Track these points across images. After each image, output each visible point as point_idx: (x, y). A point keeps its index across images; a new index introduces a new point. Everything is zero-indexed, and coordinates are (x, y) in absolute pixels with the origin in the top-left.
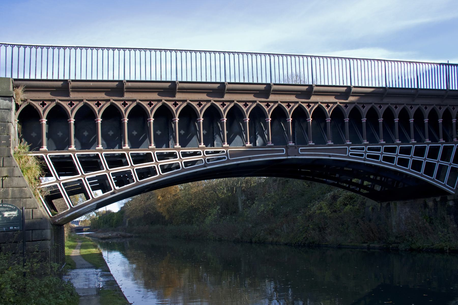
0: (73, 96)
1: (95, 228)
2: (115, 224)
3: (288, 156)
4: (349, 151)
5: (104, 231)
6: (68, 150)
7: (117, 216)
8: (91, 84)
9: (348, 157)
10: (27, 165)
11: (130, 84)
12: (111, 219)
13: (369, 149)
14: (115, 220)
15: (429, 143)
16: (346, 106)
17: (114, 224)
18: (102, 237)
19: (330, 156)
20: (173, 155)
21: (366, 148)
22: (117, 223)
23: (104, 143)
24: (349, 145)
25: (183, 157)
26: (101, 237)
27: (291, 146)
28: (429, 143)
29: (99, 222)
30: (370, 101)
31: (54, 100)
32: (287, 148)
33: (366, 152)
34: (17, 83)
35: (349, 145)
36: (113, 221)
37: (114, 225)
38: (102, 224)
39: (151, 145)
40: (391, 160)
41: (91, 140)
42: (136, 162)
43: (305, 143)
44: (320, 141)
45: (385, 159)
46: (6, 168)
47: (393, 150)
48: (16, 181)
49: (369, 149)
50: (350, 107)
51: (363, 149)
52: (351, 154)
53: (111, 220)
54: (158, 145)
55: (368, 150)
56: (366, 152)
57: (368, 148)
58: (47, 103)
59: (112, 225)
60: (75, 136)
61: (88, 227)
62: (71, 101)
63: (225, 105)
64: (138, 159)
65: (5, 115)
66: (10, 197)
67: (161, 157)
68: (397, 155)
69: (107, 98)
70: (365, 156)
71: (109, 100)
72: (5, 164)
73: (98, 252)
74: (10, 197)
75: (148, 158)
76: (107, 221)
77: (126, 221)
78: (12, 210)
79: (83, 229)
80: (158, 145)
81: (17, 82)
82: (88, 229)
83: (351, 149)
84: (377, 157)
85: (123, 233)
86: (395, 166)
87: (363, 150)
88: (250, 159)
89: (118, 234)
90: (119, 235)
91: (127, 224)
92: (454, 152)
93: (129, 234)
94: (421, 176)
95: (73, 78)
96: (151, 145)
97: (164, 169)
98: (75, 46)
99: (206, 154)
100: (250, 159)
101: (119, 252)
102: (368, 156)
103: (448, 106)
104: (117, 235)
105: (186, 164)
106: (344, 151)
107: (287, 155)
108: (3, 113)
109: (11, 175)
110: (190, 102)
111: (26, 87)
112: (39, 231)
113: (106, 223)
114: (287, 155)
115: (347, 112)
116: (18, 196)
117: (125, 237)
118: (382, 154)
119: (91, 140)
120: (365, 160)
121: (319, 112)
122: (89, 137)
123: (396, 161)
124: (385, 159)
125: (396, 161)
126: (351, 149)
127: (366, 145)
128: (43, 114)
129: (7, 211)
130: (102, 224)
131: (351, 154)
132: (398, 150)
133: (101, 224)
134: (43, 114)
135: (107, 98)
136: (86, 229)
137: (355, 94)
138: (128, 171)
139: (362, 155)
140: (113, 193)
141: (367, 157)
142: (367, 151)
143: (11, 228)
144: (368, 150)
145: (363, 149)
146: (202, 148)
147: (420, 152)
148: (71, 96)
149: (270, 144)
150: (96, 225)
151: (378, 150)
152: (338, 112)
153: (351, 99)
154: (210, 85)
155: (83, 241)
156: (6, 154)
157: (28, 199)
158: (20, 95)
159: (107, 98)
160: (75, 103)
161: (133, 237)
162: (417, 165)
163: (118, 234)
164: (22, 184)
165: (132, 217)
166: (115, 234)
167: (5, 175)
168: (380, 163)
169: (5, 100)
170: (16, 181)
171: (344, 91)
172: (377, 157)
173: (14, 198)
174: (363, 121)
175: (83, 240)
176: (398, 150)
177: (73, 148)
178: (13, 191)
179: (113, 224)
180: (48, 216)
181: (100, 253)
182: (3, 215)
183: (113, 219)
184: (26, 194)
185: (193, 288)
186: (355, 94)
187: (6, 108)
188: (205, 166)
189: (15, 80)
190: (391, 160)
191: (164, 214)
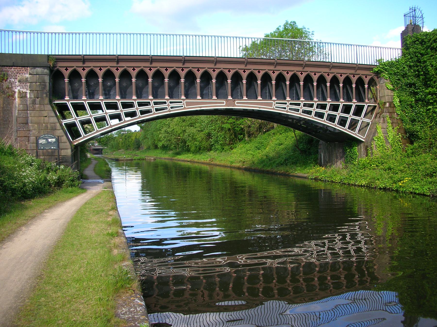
4: (275, 105)
6: (64, 99)
9: (273, 109)
13: (291, 104)
15: (356, 103)
24: (274, 101)
28: (356, 103)
33: (288, 106)
35: (274, 101)
40: (309, 113)
42: (323, 114)
44: (252, 95)
45: (304, 112)
47: (312, 106)
49: (291, 104)
51: (286, 104)
52: (276, 107)
55: (155, 104)
56: (288, 106)
57: (290, 103)
64: (125, 106)
67: (140, 104)
70: (287, 109)
78: (53, 138)
83: (276, 103)
84: (298, 110)
86: (312, 117)
98: (86, 32)
100: (260, 108)
102: (290, 109)
106: (271, 104)
118: (301, 108)
120: (287, 112)
123: (313, 114)
124: (304, 112)
125: (313, 114)
126: (276, 103)
127: (288, 101)
129: (50, 138)
132: (315, 106)
138: (60, 104)
139: (285, 108)
142: (303, 107)
144: (155, 104)
147: (335, 108)
151: (299, 105)
162: (332, 118)
168: (300, 114)
169: (45, 69)
172: (298, 110)
176: (315, 106)
177: (67, 98)
182: (48, 141)
190: (309, 113)
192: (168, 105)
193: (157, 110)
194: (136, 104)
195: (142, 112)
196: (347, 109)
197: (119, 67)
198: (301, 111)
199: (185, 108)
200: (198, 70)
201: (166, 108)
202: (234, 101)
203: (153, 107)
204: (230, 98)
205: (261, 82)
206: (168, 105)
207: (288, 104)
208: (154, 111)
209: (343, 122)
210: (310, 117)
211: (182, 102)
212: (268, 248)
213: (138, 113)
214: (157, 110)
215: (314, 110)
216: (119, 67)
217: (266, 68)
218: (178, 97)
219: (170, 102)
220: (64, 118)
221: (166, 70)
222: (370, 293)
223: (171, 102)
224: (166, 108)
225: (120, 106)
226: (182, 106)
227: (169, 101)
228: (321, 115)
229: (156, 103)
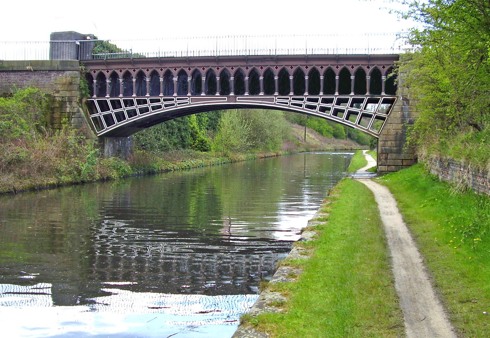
9: (275, 104)
20: (159, 101)
24: (276, 96)
27: (232, 96)
30: (267, 64)
35: (276, 96)
40: (147, 110)
45: (308, 107)
47: (316, 100)
54: (165, 95)
64: (139, 102)
67: (152, 101)
68: (319, 104)
75: (145, 102)
80: (98, 96)
83: (278, 98)
84: (301, 105)
87: (288, 99)
92: (261, 103)
97: (154, 108)
99: (177, 100)
103: (239, 66)
124: (308, 107)
139: (287, 103)
151: (302, 100)
154: (119, 60)
168: (303, 109)
174: (203, 79)
185: (25, 169)
192: (290, 101)
193: (166, 106)
194: (162, 100)
195: (154, 108)
196: (104, 106)
197: (339, 65)
198: (304, 106)
199: (190, 104)
200: (232, 68)
201: (174, 105)
202: (236, 97)
203: (162, 103)
204: (232, 94)
205: (263, 78)
206: (176, 102)
207: (305, 99)
208: (163, 106)
209: (109, 120)
210: (149, 113)
211: (187, 99)
212: (455, 247)
213: (150, 109)
214: (166, 106)
215: (319, 104)
216: (339, 65)
217: (127, 67)
218: (287, 93)
219: (177, 99)
220: (92, 113)
221: (322, 67)
222: (10, 289)
223: (178, 99)
224: (174, 105)
225: (135, 103)
226: (188, 103)
227: (176, 98)
229: (165, 100)
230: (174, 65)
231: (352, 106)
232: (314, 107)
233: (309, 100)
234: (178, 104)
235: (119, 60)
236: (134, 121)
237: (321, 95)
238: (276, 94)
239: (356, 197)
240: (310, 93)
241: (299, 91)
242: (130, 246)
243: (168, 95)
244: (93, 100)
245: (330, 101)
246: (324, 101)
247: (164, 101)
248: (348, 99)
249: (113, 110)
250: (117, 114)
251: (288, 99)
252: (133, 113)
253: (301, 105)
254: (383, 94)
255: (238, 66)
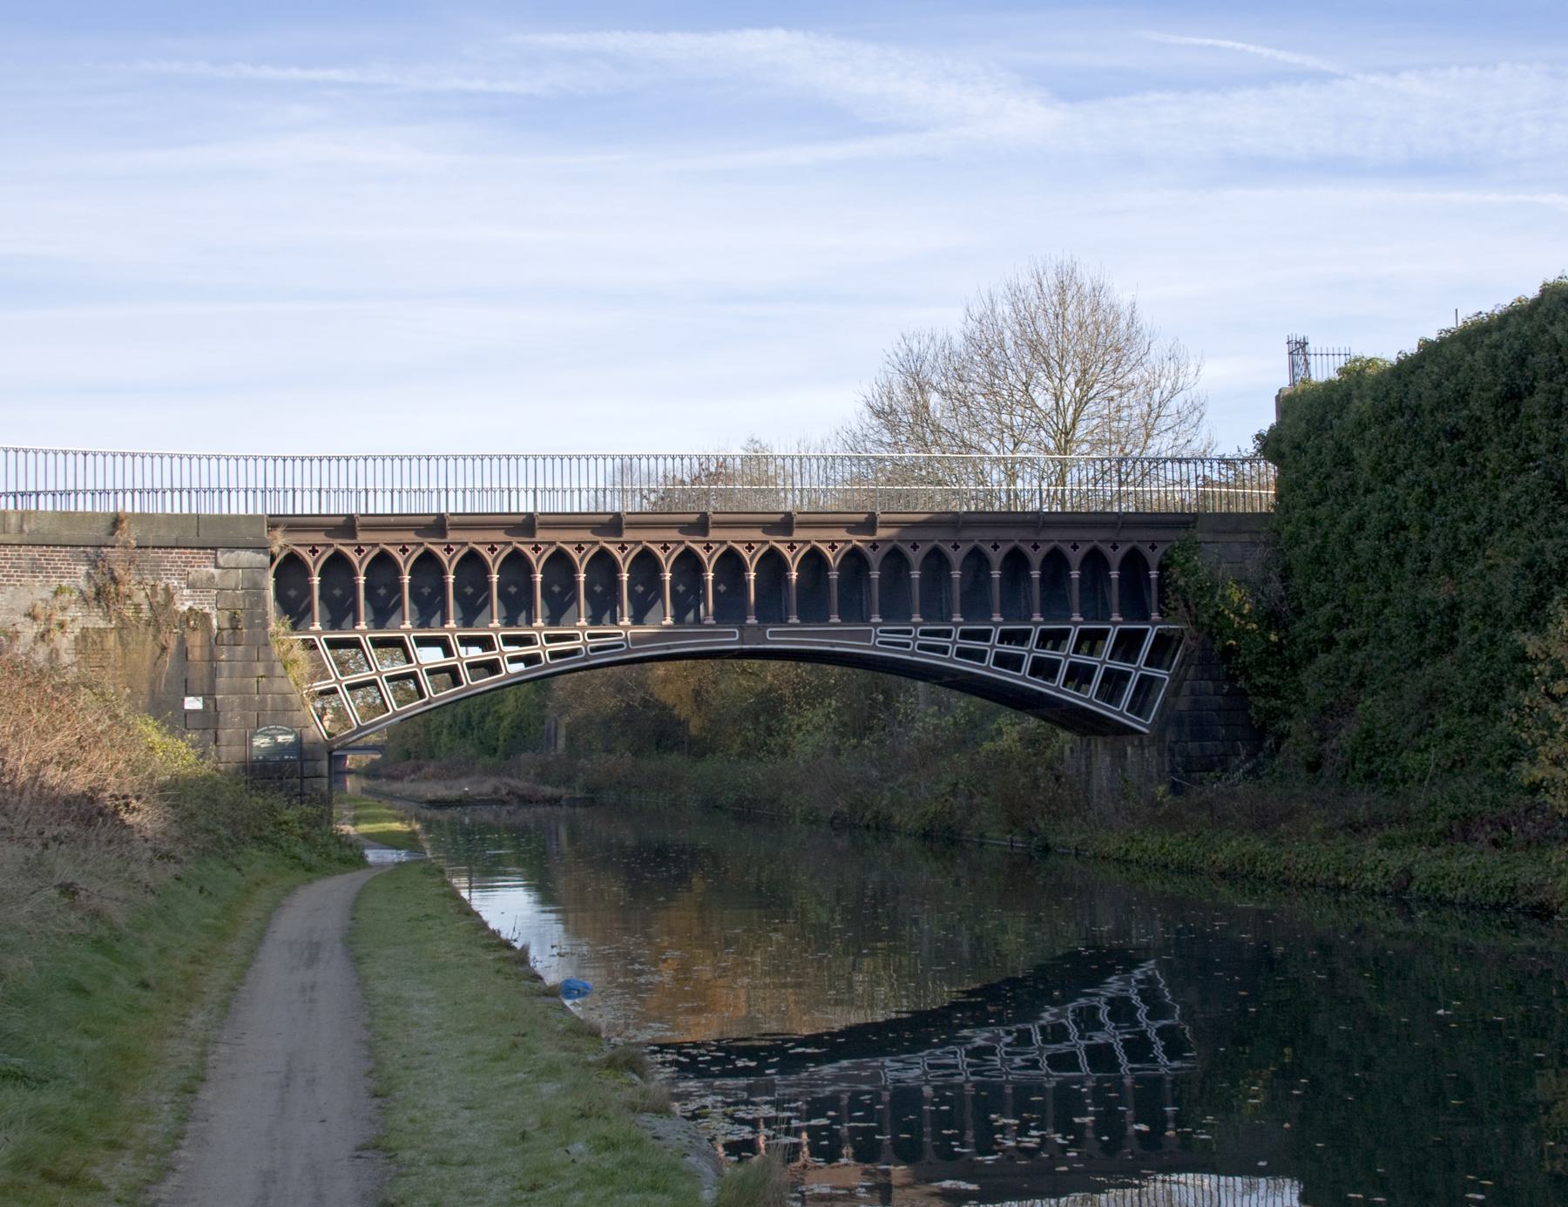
0: (362, 537)
1: (408, 756)
2: (505, 741)
3: (744, 644)
4: (877, 636)
5: (451, 772)
7: (517, 701)
8: (392, 519)
9: (874, 647)
10: (290, 656)
11: (456, 518)
12: (488, 713)
13: (923, 633)
14: (509, 719)
16: (874, 547)
17: (501, 738)
18: (433, 798)
19: (832, 645)
21: (916, 631)
22: (514, 737)
23: (415, 607)
24: (876, 625)
25: (547, 642)
26: (430, 796)
27: (751, 626)
29: (433, 727)
31: (332, 545)
32: (741, 629)
33: (915, 639)
34: (274, 522)
35: (876, 625)
36: (498, 725)
37: (501, 742)
38: (444, 738)
39: (492, 622)
41: (393, 602)
43: (783, 621)
45: (962, 653)
46: (262, 664)
47: (984, 636)
48: (278, 684)
49: (923, 633)
50: (884, 549)
52: (880, 643)
53: (489, 719)
56: (915, 639)
58: (320, 550)
59: (494, 743)
60: (366, 598)
61: (374, 748)
62: (359, 545)
63: (626, 548)
65: (259, 578)
66: (269, 708)
68: (993, 647)
69: (419, 540)
70: (914, 646)
71: (422, 544)
72: (261, 656)
73: (408, 829)
74: (269, 708)
76: (469, 723)
77: (556, 728)
78: (287, 733)
79: (344, 757)
81: (273, 519)
82: (373, 761)
83: (881, 632)
84: (945, 650)
85: (521, 785)
88: (668, 647)
89: (503, 787)
90: (504, 792)
91: (561, 743)
93: (548, 790)
94: (1057, 692)
95: (363, 512)
96: (492, 622)
100: (668, 647)
101: (553, 916)
102: (921, 647)
104: (496, 790)
105: (554, 655)
106: (866, 636)
107: (742, 641)
108: (256, 574)
109: (270, 674)
110: (562, 545)
111: (289, 526)
112: (312, 763)
113: (464, 734)
114: (742, 641)
115: (875, 558)
116: (281, 708)
117: (531, 802)
119: (393, 602)
121: (814, 560)
122: (388, 597)
124: (962, 653)
126: (881, 632)
127: (916, 625)
128: (314, 568)
129: (281, 734)
130: (444, 738)
131: (880, 643)
132: (995, 636)
133: (439, 734)
134: (314, 568)
135: (419, 539)
136: (358, 757)
137: (887, 525)
139: (907, 645)
140: (428, 703)
141: (919, 648)
143: (286, 757)
145: (909, 632)
146: (582, 628)
147: (1053, 638)
148: (359, 538)
149: (711, 621)
150: (416, 740)
151: (948, 634)
152: (855, 556)
153: (882, 533)
155: (356, 807)
156: (262, 641)
157: (295, 713)
158: (280, 542)
159: (419, 540)
160: (366, 549)
161: (562, 802)
163: (503, 787)
164: (286, 688)
165: (580, 711)
166: (487, 786)
167: (262, 674)
168: (951, 660)
170: (278, 684)
171: (863, 520)
173: (275, 710)
175: (358, 804)
176: (995, 636)
178: (273, 699)
179: (498, 739)
180: (320, 736)
181: (410, 833)
182: (276, 740)
183: (496, 712)
184: (292, 705)
186: (887, 525)
187: (259, 566)
188: (585, 660)
189: (271, 516)
191: (683, 711)
204: (752, 620)
228: (1012, 662)
229: (550, 639)
230: (1075, 534)
231: (1077, 650)
232: (979, 656)
233: (965, 635)
234: (921, 647)
235: (334, 519)
236: (1041, 693)
237: (997, 623)
238: (876, 619)
239: (1343, 855)
240: (927, 617)
241: (935, 609)
242: (768, 1043)
243: (1095, 619)
244: (313, 640)
245: (1021, 637)
246: (1006, 637)
247: (547, 642)
248: (1107, 631)
249: (1105, 666)
250: (1091, 670)
251: (909, 632)
252: (1044, 669)
253: (945, 650)
254: (1116, 617)
255: (973, 541)
